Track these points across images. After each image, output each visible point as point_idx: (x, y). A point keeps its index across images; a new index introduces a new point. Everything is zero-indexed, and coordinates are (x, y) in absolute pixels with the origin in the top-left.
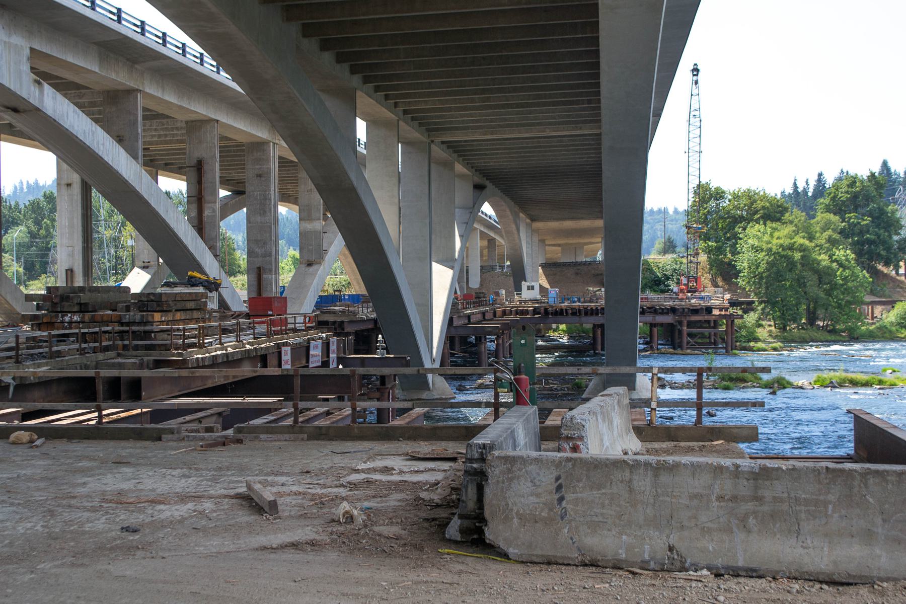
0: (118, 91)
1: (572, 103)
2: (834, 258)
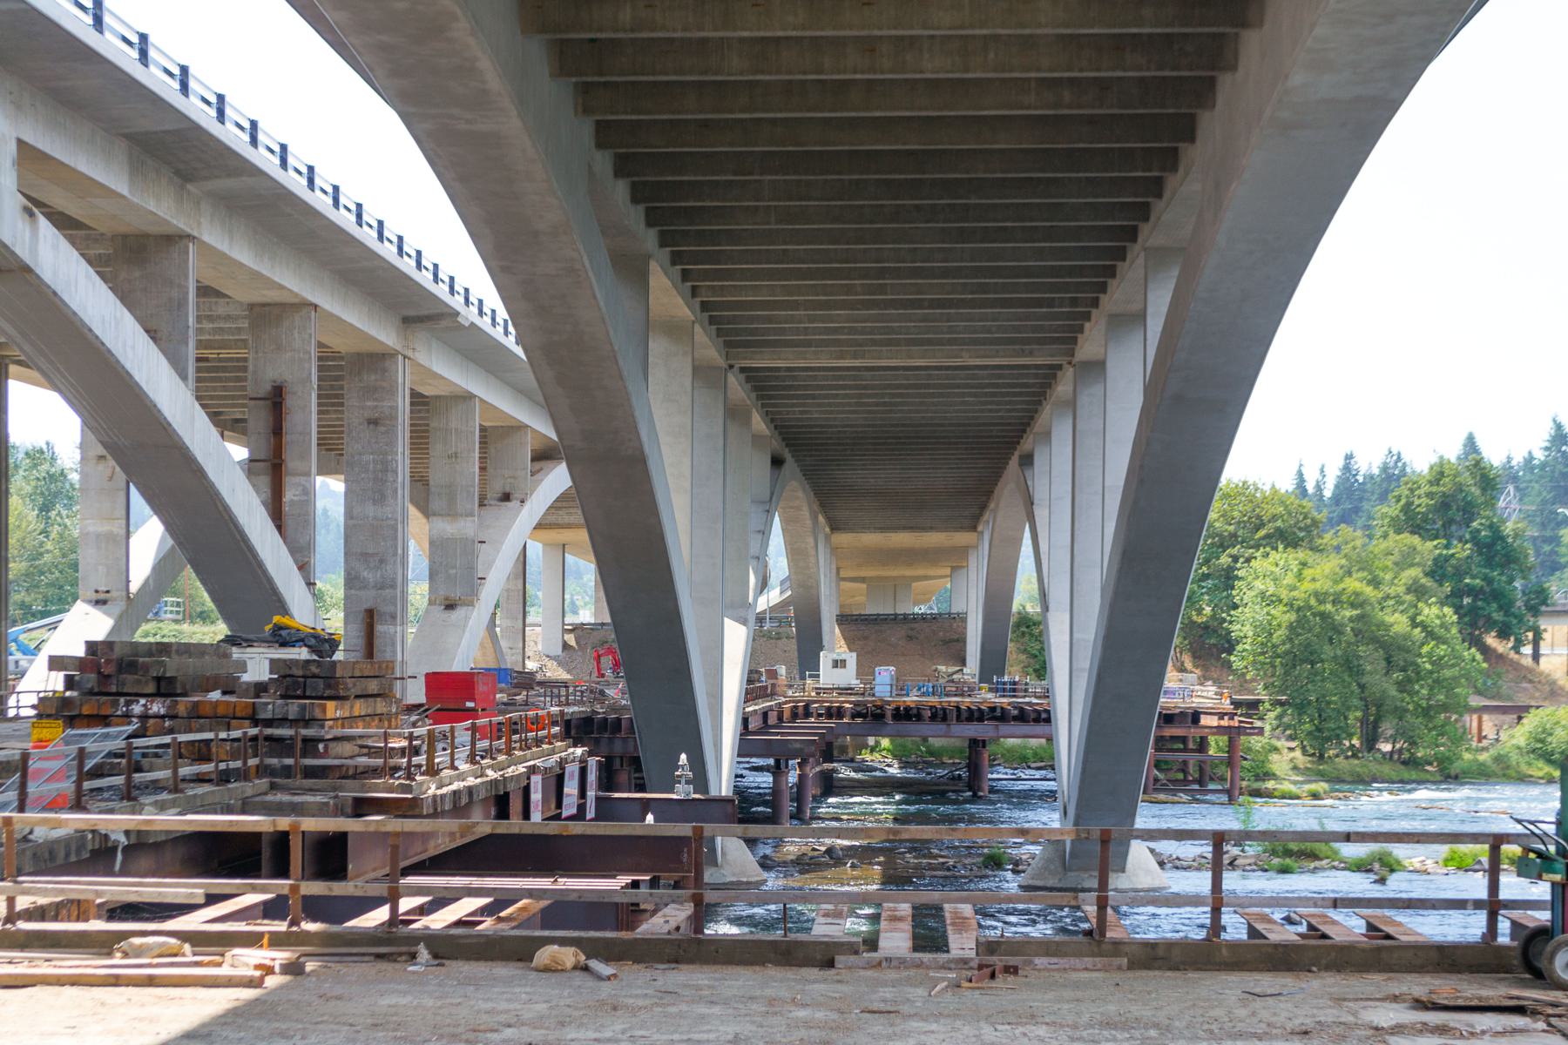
0: (146, 236)
1: (1039, 303)
2: (1419, 619)
